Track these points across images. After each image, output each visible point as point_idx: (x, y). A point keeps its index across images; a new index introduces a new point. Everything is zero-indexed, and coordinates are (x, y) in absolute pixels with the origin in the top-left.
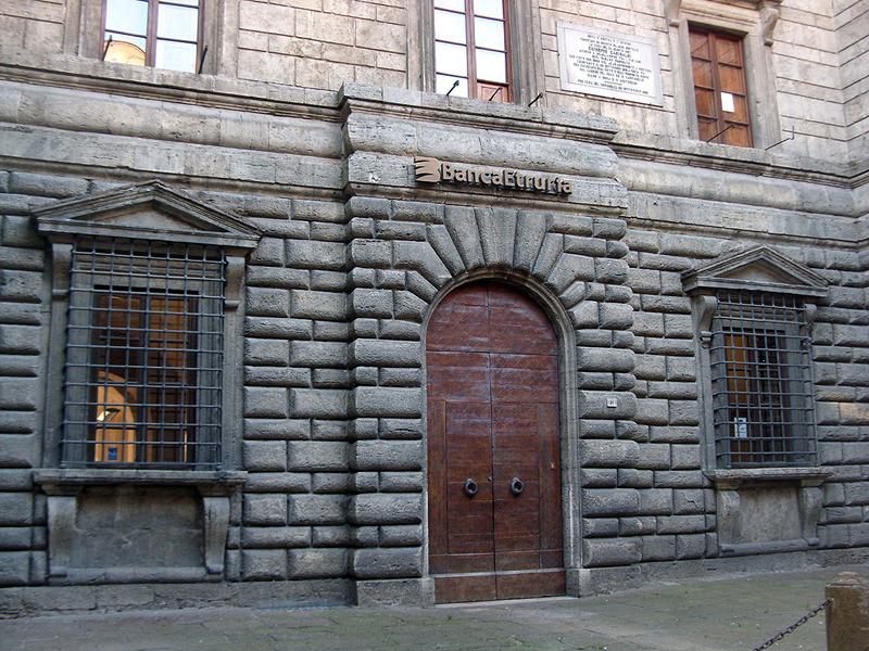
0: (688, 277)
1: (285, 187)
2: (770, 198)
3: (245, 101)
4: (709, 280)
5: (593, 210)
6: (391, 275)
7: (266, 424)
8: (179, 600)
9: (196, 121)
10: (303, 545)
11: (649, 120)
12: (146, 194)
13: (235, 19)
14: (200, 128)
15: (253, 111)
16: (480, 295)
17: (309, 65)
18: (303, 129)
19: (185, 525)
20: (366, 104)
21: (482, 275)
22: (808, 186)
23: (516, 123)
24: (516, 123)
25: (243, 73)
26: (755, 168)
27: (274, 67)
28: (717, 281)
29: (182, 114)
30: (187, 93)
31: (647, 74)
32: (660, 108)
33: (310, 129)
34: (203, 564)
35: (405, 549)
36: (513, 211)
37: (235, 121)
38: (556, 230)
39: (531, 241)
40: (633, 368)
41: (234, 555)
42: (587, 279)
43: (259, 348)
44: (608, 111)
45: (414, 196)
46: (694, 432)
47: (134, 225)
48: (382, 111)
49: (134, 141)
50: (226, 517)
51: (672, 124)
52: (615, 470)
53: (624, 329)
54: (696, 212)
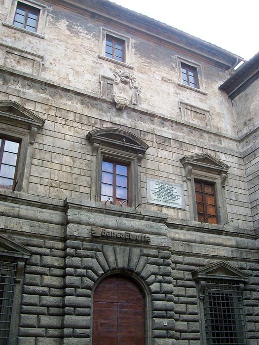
0: (194, 273)
2: (225, 243)
3: (30, 202)
5: (159, 248)
11: (180, 214)
20: (75, 205)
21: (116, 272)
22: (239, 239)
26: (219, 232)
27: (41, 190)
29: (6, 205)
31: (179, 197)
32: (184, 210)
36: (128, 248)
37: (26, 209)
38: (144, 255)
39: (135, 259)
42: (156, 274)
43: (28, 298)
44: (165, 211)
45: (91, 241)
48: (80, 209)
51: (188, 216)
54: (197, 249)
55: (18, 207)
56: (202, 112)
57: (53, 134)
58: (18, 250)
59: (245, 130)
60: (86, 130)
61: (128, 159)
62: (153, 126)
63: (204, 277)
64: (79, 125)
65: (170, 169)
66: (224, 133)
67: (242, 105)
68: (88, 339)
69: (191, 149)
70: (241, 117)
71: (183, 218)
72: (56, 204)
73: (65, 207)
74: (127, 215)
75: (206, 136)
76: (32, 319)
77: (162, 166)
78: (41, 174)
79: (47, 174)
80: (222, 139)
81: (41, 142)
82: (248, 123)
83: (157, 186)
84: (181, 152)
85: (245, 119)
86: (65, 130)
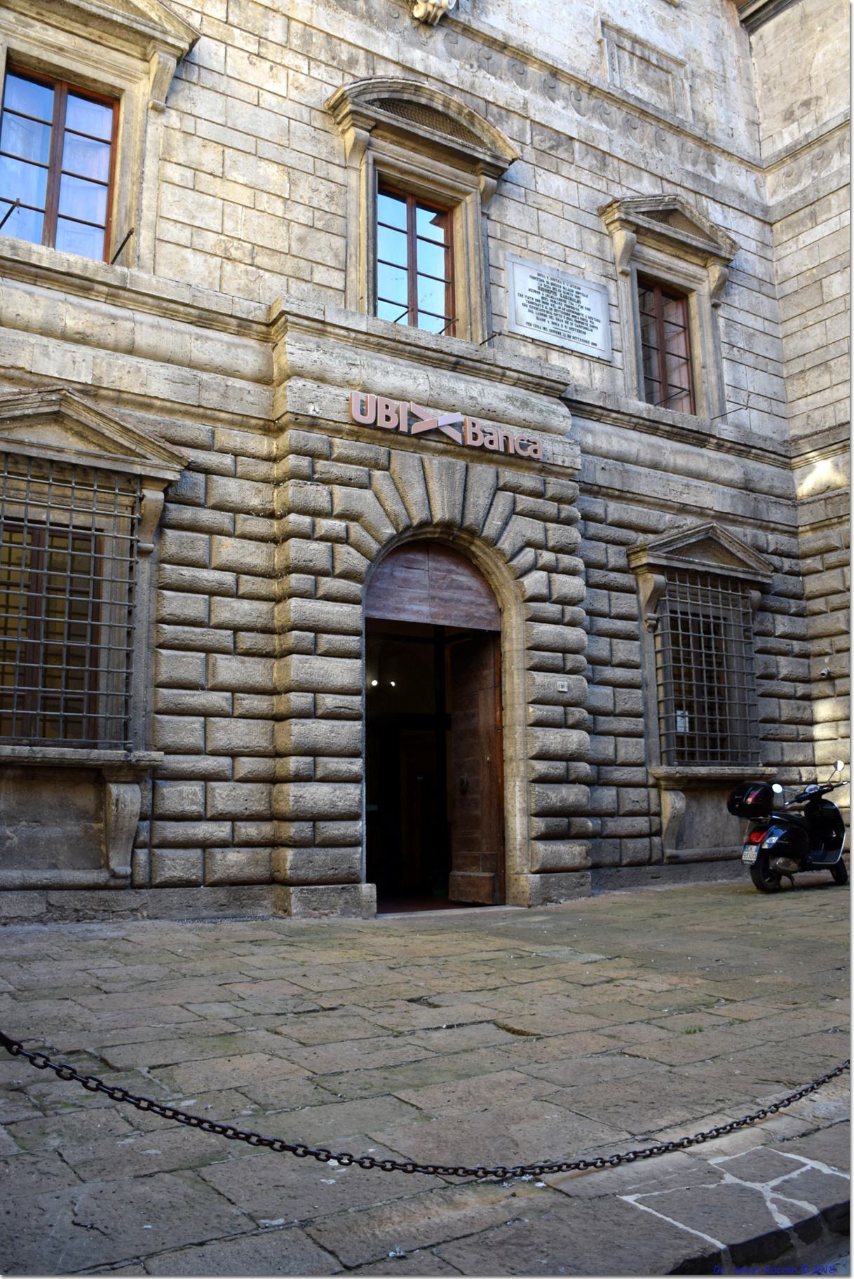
1: (209, 412)
2: (714, 473)
3: (165, 304)
4: (659, 557)
6: (325, 525)
7: (181, 695)
8: (76, 910)
9: (108, 321)
10: (224, 844)
11: (597, 375)
12: (51, 403)
13: (155, 204)
14: (111, 330)
15: (172, 318)
16: (420, 557)
17: (238, 270)
18: (230, 345)
19: (83, 818)
20: (306, 322)
21: (429, 533)
22: (752, 464)
23: (466, 362)
24: (466, 362)
25: (163, 270)
26: (699, 438)
27: (198, 268)
28: (666, 558)
29: (90, 311)
30: (97, 287)
31: (596, 324)
32: (608, 363)
33: (237, 346)
34: (107, 866)
35: (343, 850)
37: (153, 326)
38: (505, 488)
39: (479, 497)
40: (583, 649)
41: (142, 855)
43: (175, 603)
44: (555, 359)
46: (639, 724)
47: (34, 440)
48: (322, 333)
49: (34, 339)
50: (136, 808)
51: (620, 382)
52: (564, 764)
53: (574, 605)
54: (646, 483)
55: (127, 319)
56: (665, 64)
57: (223, 85)
58: (142, 452)
59: (786, 135)
60: (328, 84)
61: (453, 188)
62: (521, 92)
63: (664, 562)
64: (302, 63)
65: (569, 234)
66: (722, 140)
67: (785, 52)
68: (359, 698)
69: (631, 178)
70: (776, 93)
71: (606, 386)
72: (244, 316)
73: (269, 329)
74: (457, 363)
75: (672, 141)
76: (188, 665)
77: (549, 224)
78: (194, 217)
79: (213, 215)
80: (720, 159)
81: (186, 106)
82: (798, 113)
83: (534, 285)
84: (602, 185)
85: (790, 98)
86: (259, 74)
